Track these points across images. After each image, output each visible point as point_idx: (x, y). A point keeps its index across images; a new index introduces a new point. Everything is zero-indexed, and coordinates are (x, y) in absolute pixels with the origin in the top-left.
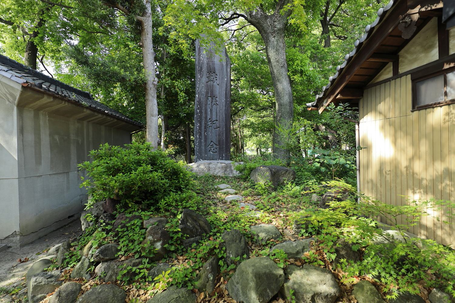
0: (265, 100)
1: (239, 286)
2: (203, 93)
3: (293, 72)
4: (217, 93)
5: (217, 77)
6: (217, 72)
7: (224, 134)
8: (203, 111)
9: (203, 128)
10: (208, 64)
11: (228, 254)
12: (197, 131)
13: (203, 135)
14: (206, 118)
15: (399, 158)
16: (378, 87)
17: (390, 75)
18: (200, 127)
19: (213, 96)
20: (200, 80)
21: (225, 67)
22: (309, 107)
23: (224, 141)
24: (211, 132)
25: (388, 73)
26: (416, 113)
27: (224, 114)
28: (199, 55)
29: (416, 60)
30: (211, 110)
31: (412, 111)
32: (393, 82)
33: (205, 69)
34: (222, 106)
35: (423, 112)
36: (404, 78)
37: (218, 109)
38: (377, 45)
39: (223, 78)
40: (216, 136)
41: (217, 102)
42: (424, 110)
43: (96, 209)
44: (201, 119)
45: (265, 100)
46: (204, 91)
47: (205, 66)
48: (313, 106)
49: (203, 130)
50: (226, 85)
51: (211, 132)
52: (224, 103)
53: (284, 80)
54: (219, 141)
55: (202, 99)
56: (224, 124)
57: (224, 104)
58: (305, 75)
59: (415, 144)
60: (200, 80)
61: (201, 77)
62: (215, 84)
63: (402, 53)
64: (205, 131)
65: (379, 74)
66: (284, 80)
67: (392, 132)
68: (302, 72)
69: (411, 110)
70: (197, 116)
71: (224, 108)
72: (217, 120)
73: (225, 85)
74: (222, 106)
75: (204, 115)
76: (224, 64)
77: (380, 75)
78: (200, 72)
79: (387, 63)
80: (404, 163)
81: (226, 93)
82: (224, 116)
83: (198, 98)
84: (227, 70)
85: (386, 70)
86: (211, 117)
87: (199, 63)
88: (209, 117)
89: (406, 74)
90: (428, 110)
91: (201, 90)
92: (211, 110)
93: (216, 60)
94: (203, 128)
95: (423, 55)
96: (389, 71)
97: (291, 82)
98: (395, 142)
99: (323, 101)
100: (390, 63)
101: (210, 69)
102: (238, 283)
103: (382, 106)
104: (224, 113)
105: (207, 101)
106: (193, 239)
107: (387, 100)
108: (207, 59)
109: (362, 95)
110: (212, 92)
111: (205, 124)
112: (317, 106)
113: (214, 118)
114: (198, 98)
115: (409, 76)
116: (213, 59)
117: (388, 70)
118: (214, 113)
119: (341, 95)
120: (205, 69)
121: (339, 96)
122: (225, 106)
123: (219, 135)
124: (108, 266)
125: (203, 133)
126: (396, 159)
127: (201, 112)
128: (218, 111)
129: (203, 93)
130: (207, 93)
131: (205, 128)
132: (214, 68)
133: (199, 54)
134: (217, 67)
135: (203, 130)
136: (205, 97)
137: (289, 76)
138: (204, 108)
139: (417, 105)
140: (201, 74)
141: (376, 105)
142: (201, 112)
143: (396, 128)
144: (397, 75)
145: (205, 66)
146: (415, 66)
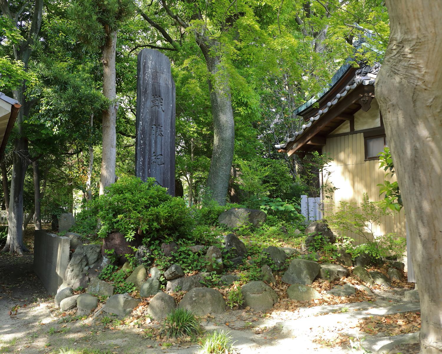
0: (192, 129)
1: (294, 275)
2: (148, 120)
3: (237, 103)
4: (163, 121)
5: (163, 101)
6: (163, 96)
7: (169, 172)
8: (147, 142)
9: (147, 163)
10: (153, 85)
11: (276, 261)
12: (140, 167)
13: (146, 172)
14: (150, 151)
15: (356, 198)
16: (335, 138)
17: (348, 130)
18: (144, 162)
19: (158, 125)
20: (144, 104)
21: (171, 90)
22: (279, 149)
23: (169, 181)
24: (156, 170)
25: (345, 128)
26: (367, 162)
27: (169, 147)
28: (144, 74)
29: (366, 123)
30: (156, 142)
31: (365, 161)
32: (350, 136)
33: (149, 91)
34: (167, 138)
35: (372, 161)
36: (358, 135)
37: (163, 141)
38: (344, 109)
39: (168, 104)
40: (161, 174)
41: (162, 133)
42: (373, 161)
43: (91, 251)
44: (145, 152)
45: (192, 129)
46: (148, 117)
47: (150, 88)
48: (282, 148)
49: (147, 166)
50: (172, 112)
51: (156, 170)
52: (169, 134)
53: (228, 111)
54: (164, 181)
55: (146, 128)
56: (169, 160)
57: (169, 135)
58: (250, 108)
59: (368, 186)
60: (144, 104)
61: (146, 100)
62: (160, 110)
63: (356, 115)
64: (149, 168)
65: (338, 128)
66: (228, 111)
67: (351, 176)
68: (246, 105)
69: (364, 159)
70: (141, 148)
71: (169, 140)
72: (161, 155)
73: (170, 113)
74: (167, 138)
75: (147, 148)
76: (170, 87)
77: (340, 129)
78: (145, 95)
79: (344, 121)
80: (360, 201)
81: (171, 121)
82: (169, 150)
83: (142, 126)
84: (172, 94)
85: (344, 125)
86: (156, 150)
87: (143, 83)
88: (153, 150)
89: (360, 132)
90: (376, 161)
91: (145, 116)
92: (156, 142)
93: (162, 82)
94: (147, 163)
95: (371, 120)
96: (347, 127)
97: (235, 114)
98: (353, 185)
99: (293, 145)
100: (347, 121)
101: (156, 92)
102: (292, 273)
103: (342, 156)
104: (169, 146)
105: (151, 130)
106: (236, 258)
107: (347, 150)
108: (153, 79)
109: (325, 143)
110: (157, 119)
111: (149, 158)
112: (286, 149)
113: (159, 153)
114: (142, 126)
115: (362, 134)
116: (158, 80)
117: (346, 125)
118: (159, 146)
119: (311, 142)
120: (149, 91)
121: (309, 143)
122: (171, 138)
123: (164, 174)
124: (181, 281)
125: (146, 169)
126: (354, 199)
127: (144, 143)
128: (163, 144)
129: (148, 120)
130: (152, 120)
131: (149, 163)
132: (160, 91)
133: (144, 72)
134: (163, 90)
135: (147, 166)
136: (150, 125)
137: (233, 108)
138: (148, 139)
139: (369, 157)
140: (145, 97)
141: (338, 154)
142: (144, 143)
143: (357, 175)
144: (353, 131)
145: (150, 88)
146: (366, 127)
